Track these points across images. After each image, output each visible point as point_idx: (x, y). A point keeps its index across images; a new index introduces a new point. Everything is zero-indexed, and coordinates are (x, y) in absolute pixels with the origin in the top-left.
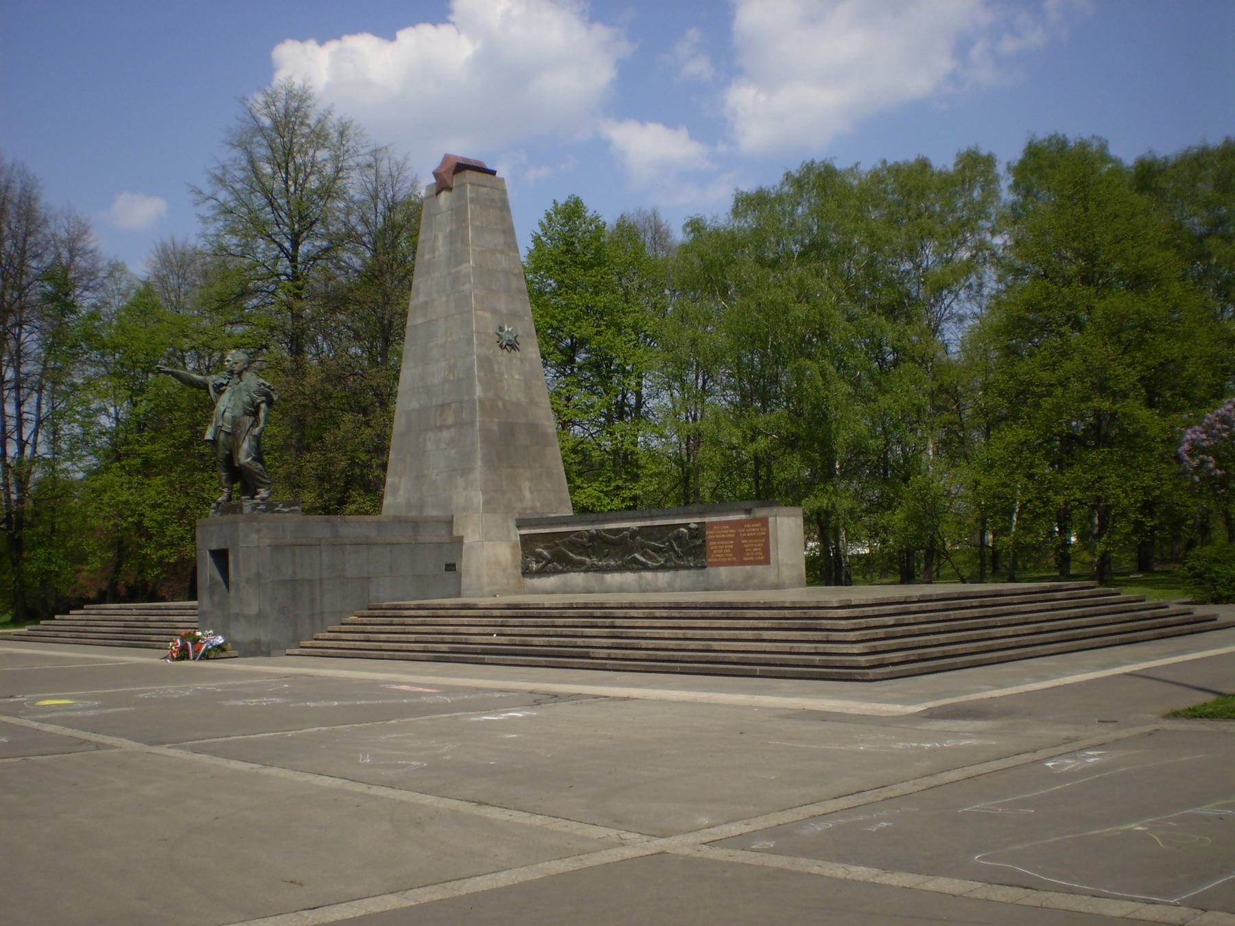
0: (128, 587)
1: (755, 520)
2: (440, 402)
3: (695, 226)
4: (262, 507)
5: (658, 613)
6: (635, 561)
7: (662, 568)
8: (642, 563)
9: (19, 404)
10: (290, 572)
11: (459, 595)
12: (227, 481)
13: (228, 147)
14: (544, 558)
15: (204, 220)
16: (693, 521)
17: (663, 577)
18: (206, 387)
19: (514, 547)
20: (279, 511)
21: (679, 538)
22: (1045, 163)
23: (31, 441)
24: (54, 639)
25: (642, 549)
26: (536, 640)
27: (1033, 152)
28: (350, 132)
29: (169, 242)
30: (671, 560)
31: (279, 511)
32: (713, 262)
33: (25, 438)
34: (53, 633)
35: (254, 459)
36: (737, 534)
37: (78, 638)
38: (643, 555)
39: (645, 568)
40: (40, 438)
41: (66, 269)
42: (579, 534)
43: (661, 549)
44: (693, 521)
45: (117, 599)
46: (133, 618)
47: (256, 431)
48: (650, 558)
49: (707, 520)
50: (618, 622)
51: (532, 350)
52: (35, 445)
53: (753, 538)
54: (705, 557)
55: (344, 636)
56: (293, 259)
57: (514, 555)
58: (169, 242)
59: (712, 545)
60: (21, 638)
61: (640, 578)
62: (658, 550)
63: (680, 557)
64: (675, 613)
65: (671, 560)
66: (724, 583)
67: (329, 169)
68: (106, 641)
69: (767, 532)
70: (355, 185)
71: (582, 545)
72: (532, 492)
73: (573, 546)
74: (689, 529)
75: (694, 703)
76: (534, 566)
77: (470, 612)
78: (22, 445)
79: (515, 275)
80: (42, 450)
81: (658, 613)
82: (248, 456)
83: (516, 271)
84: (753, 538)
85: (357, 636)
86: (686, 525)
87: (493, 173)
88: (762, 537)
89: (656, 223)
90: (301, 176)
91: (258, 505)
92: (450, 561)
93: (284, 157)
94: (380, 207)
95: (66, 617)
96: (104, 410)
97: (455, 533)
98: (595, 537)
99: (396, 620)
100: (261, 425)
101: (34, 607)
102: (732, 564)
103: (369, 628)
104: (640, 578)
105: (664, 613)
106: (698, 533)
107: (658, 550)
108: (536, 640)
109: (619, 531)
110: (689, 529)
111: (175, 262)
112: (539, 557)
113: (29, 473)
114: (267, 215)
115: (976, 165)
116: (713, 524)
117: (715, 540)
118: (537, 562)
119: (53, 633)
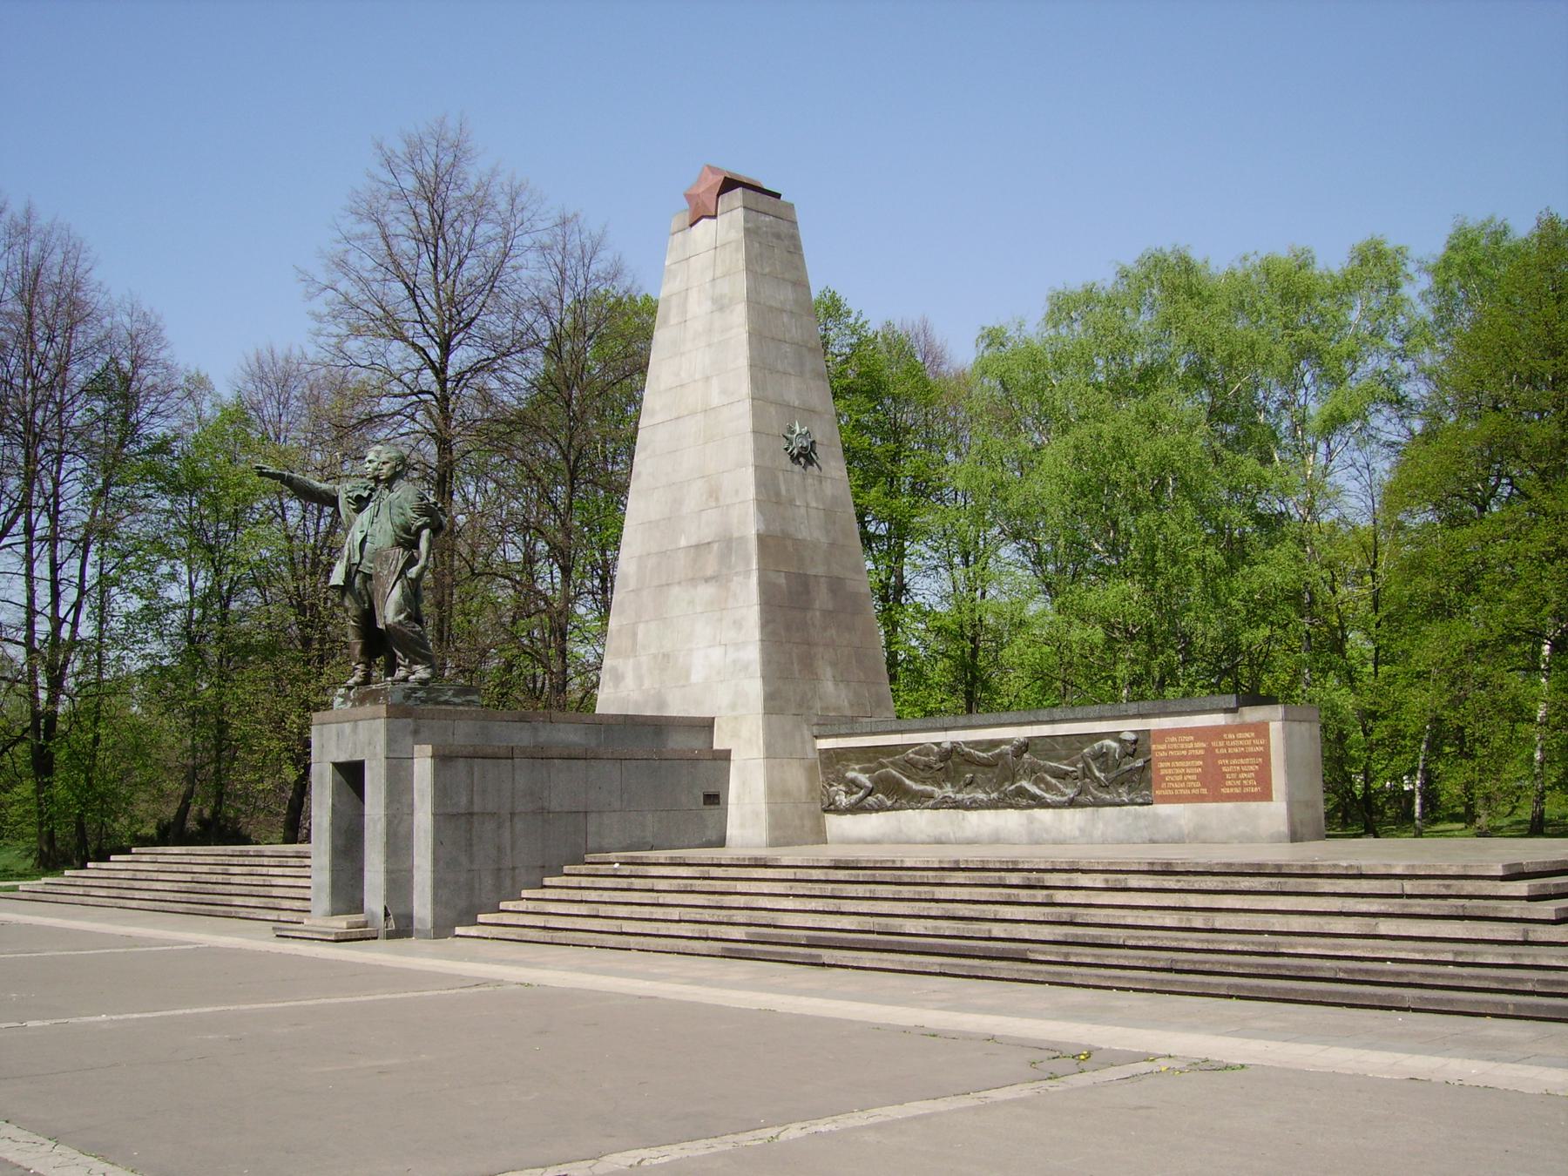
0: (201, 821)
1: (1243, 727)
2: (693, 541)
3: (993, 338)
4: (420, 694)
5: (1134, 881)
6: (1021, 792)
7: (1072, 804)
8: (1034, 797)
9: (55, 567)
10: (464, 800)
11: (721, 843)
12: (363, 652)
13: (353, 218)
14: (860, 787)
15: (318, 318)
16: (1128, 727)
17: (1072, 820)
18: (333, 501)
19: (810, 770)
20: (447, 703)
21: (1102, 756)
22: (1472, 262)
23: (70, 618)
24: (84, 901)
25: (1034, 773)
26: (910, 926)
27: (1463, 242)
28: (523, 199)
29: (266, 355)
30: (1087, 792)
31: (447, 703)
32: (1023, 387)
33: (62, 615)
34: (81, 891)
35: (408, 617)
36: (1210, 750)
37: (120, 897)
38: (1036, 783)
39: (1042, 804)
40: (83, 617)
41: (127, 380)
42: (923, 750)
43: (1067, 773)
44: (1128, 727)
45: (184, 839)
46: (205, 869)
47: (413, 572)
48: (1049, 788)
49: (1154, 724)
50: (1061, 896)
51: (834, 467)
52: (75, 624)
53: (1239, 756)
54: (1149, 787)
55: (552, 907)
56: (440, 371)
57: (811, 780)
58: (266, 355)
59: (1163, 768)
60: (34, 898)
61: (1031, 820)
62: (1062, 776)
63: (1102, 787)
64: (1170, 882)
65: (1087, 792)
66: (1179, 825)
67: (493, 250)
68: (161, 907)
69: (1267, 746)
70: (531, 274)
71: (928, 766)
72: (836, 683)
73: (910, 767)
74: (1121, 741)
75: (1331, 1081)
76: (843, 800)
77: (770, 873)
78: (57, 623)
79: (810, 349)
80: (86, 630)
81: (1134, 881)
82: (399, 612)
83: (812, 344)
84: (1239, 756)
85: (574, 909)
86: (1115, 736)
87: (778, 196)
88: (1256, 755)
89: (927, 343)
90: (455, 262)
91: (414, 690)
92: (712, 790)
93: (434, 236)
94: (568, 300)
95: (104, 865)
96: (173, 577)
97: (716, 747)
98: (951, 754)
99: (638, 883)
100: (421, 562)
101: (71, 843)
102: (1201, 798)
103: (593, 895)
104: (1031, 820)
105: (1149, 882)
106: (1137, 747)
107: (1062, 776)
108: (910, 926)
109: (994, 744)
110: (1121, 741)
111: (277, 379)
112: (852, 786)
113: (67, 661)
114: (406, 311)
115: (1377, 264)
116: (1163, 734)
117: (1169, 759)
118: (849, 793)
119: (81, 891)
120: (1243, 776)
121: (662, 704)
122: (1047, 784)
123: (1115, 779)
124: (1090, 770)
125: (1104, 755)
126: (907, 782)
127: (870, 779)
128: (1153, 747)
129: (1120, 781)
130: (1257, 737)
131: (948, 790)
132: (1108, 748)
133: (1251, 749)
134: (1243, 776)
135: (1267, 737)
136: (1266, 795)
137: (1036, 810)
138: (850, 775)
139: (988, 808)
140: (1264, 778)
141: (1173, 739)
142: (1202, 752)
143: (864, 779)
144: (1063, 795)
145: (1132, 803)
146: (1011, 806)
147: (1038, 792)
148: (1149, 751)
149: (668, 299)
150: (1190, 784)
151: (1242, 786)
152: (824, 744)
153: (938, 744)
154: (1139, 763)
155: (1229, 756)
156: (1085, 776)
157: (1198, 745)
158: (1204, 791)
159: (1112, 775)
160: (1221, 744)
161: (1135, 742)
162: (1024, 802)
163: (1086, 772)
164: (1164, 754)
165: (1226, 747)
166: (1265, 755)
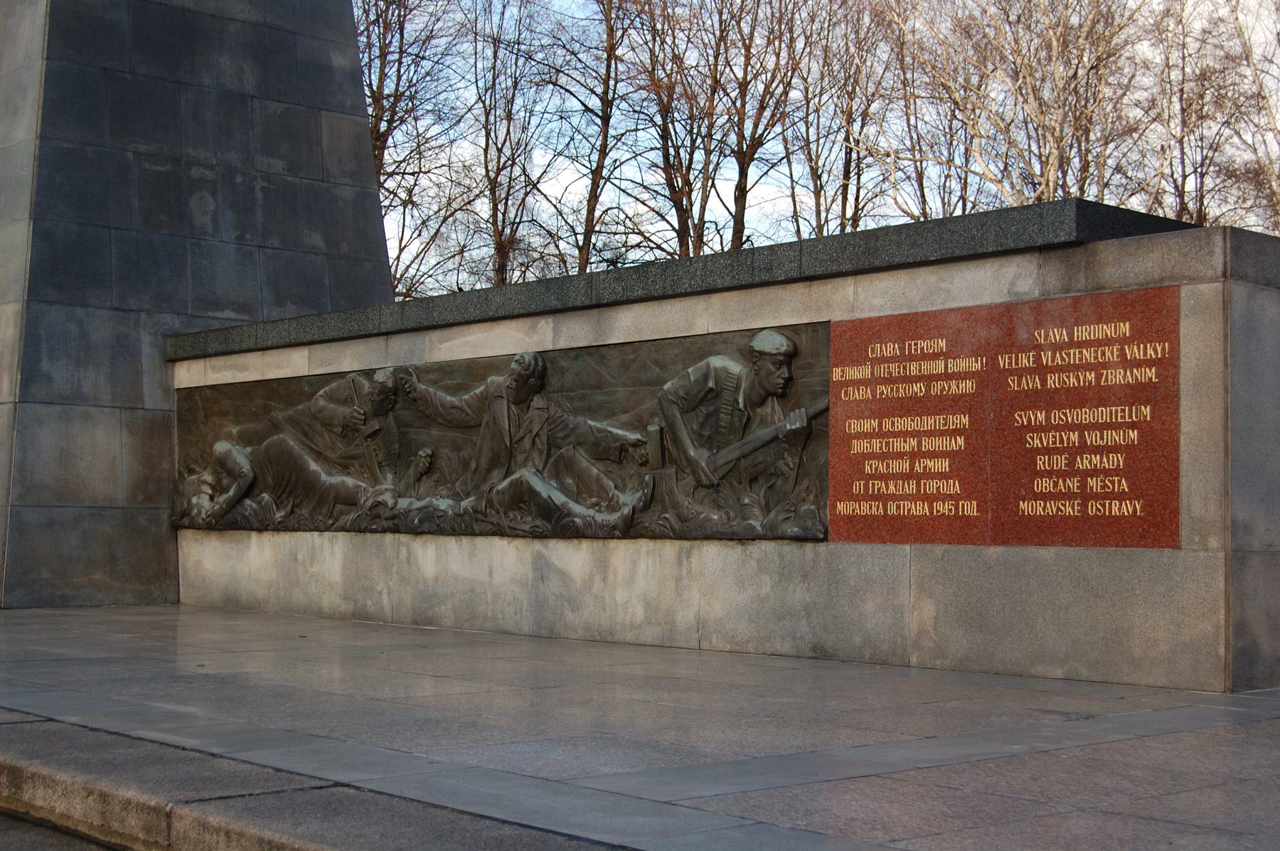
6: (522, 497)
7: (630, 529)
14: (233, 474)
21: (706, 397)
36: (990, 379)
63: (711, 488)
69: (1168, 366)
88: (1136, 394)
104: (542, 567)
107: (614, 454)
110: (753, 357)
116: (866, 332)
120: (1083, 463)
121: (331, 541)
122: (579, 476)
123: (734, 467)
124: (676, 440)
125: (711, 396)
126: (313, 466)
127: (253, 458)
128: (837, 374)
129: (750, 473)
130: (1139, 336)
131: (386, 490)
132: (722, 374)
133: (1116, 377)
134: (1083, 463)
135: (1169, 334)
136: (1158, 525)
137: (552, 543)
138: (221, 447)
139: (454, 532)
140: (1154, 465)
141: (891, 349)
142: (968, 386)
143: (241, 458)
144: (613, 507)
145: (772, 535)
146: (500, 532)
147: (559, 498)
148: (827, 385)
149: (17, 301)
150: (932, 486)
151: (1085, 496)
152: (189, 375)
153: (369, 373)
154: (796, 421)
155: (1048, 399)
156: (665, 458)
157: (962, 365)
158: (970, 508)
159: (727, 455)
160: (1026, 361)
161: (790, 357)
162: (527, 523)
163: (668, 453)
164: (864, 393)
165: (1041, 370)
166: (1162, 395)
